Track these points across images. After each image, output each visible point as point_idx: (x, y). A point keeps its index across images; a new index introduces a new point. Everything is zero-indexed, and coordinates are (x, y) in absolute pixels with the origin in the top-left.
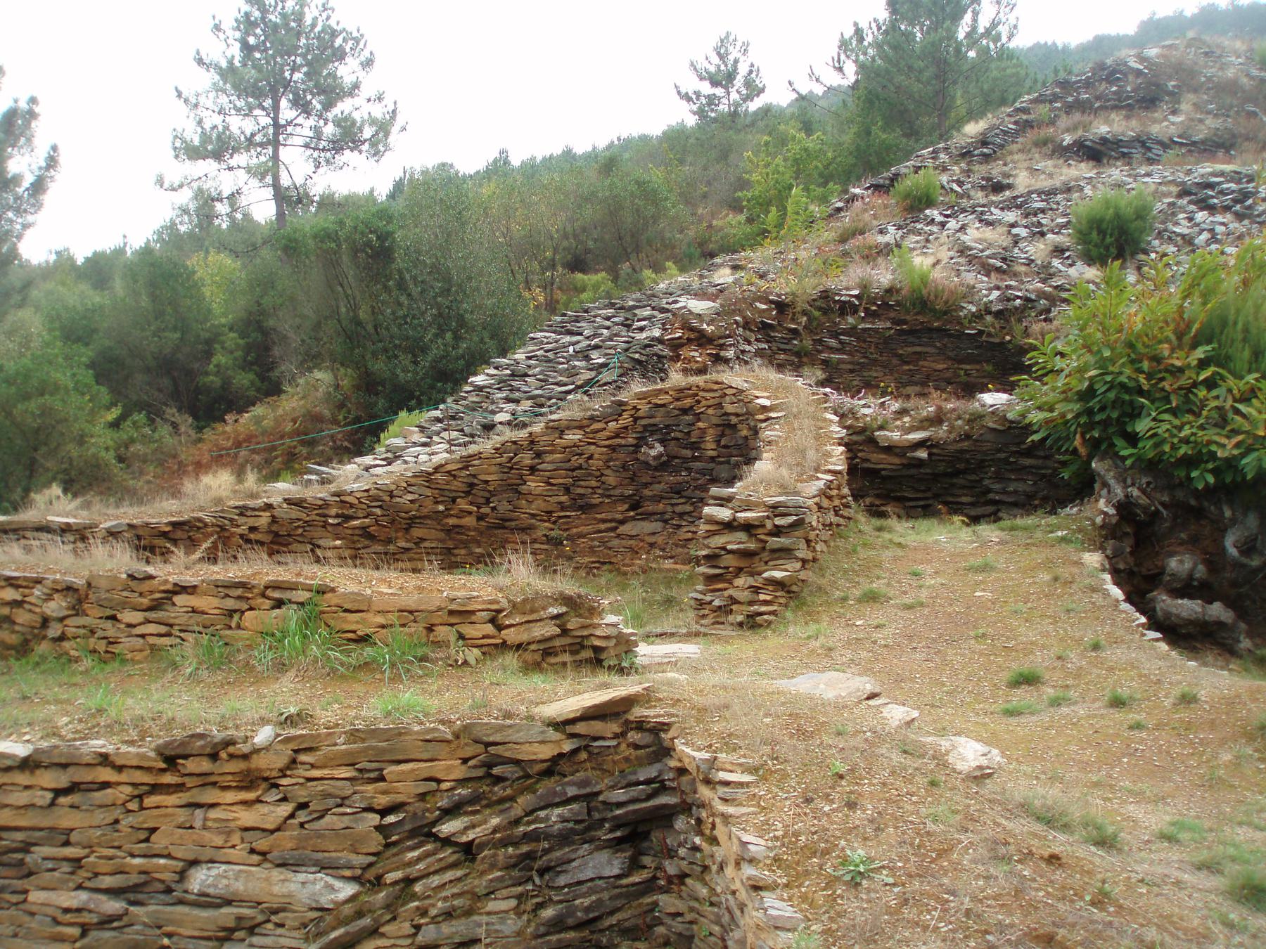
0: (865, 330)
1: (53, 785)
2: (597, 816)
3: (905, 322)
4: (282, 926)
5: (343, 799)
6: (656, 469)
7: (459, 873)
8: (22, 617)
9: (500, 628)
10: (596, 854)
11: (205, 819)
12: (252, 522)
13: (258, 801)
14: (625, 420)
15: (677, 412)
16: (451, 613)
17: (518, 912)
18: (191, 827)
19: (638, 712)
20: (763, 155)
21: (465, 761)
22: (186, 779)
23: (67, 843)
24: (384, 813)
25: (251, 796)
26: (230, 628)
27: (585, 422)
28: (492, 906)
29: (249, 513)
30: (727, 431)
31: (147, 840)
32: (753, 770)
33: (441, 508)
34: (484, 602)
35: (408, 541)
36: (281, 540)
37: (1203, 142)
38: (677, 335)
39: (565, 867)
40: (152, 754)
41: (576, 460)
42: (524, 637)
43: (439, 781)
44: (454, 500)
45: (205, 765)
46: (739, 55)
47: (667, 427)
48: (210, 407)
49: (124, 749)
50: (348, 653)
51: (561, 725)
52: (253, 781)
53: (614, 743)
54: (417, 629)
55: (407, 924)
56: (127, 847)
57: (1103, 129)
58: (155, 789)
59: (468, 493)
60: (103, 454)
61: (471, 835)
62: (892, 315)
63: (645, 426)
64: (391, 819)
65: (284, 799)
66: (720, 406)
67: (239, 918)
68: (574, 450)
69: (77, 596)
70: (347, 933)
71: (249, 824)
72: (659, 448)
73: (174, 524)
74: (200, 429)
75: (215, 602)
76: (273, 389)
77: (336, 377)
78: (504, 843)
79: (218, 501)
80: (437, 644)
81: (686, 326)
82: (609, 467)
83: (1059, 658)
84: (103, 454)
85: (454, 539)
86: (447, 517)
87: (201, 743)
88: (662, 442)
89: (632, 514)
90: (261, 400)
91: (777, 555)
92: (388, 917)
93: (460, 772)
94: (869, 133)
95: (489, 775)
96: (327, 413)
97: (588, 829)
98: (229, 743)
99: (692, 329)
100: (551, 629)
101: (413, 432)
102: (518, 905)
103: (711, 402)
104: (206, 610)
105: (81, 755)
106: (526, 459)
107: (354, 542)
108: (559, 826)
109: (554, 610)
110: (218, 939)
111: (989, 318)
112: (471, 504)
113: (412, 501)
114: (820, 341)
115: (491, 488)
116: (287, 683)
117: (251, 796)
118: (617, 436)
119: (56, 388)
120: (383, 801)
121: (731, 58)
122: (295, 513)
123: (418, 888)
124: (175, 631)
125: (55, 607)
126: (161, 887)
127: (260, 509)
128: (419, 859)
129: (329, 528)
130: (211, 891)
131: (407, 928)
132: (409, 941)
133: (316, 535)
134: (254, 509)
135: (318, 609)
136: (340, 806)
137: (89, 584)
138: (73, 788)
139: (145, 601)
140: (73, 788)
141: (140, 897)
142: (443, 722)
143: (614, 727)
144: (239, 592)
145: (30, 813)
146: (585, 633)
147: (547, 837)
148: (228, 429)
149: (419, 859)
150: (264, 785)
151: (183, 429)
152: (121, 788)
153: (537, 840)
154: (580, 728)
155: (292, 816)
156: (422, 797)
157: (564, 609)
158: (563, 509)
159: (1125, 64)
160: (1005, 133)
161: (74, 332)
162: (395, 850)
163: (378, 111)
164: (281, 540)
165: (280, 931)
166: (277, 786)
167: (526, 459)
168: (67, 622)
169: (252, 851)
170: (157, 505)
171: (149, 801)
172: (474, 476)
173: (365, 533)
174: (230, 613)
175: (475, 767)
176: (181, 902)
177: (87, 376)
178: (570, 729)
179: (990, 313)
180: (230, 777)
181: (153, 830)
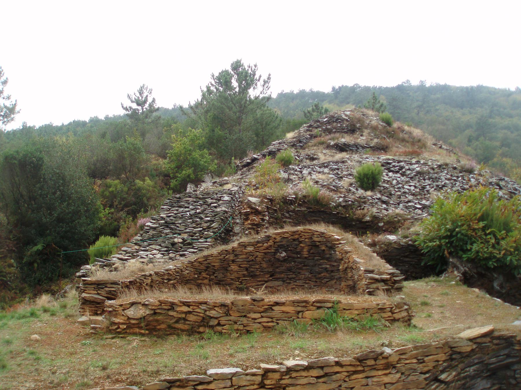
0: (298, 211)
3: (311, 208)
6: (282, 261)
9: (393, 313)
13: (390, 373)
14: (271, 243)
18: (367, 385)
20: (179, 137)
21: (445, 353)
25: (388, 371)
26: (298, 318)
30: (313, 248)
37: (373, 147)
41: (251, 258)
44: (200, 273)
45: (372, 362)
46: (148, 94)
47: (287, 245)
51: (471, 340)
52: (389, 366)
57: (343, 140)
58: (355, 372)
59: (206, 270)
62: (306, 205)
66: (311, 238)
68: (250, 253)
71: (387, 382)
75: (293, 308)
78: (457, 381)
86: (198, 280)
87: (373, 354)
88: (285, 251)
89: (271, 278)
94: (213, 131)
99: (252, 208)
103: (307, 237)
104: (289, 311)
105: (330, 362)
108: (473, 373)
111: (340, 208)
112: (207, 274)
114: (283, 214)
115: (216, 268)
117: (388, 371)
120: (426, 369)
121: (144, 95)
124: (274, 320)
138: (326, 375)
143: (489, 339)
144: (304, 304)
152: (343, 373)
154: (479, 340)
158: (244, 277)
159: (341, 116)
160: (307, 138)
163: (8, 104)
167: (231, 257)
174: (299, 312)
178: (474, 341)
179: (341, 206)
180: (381, 366)
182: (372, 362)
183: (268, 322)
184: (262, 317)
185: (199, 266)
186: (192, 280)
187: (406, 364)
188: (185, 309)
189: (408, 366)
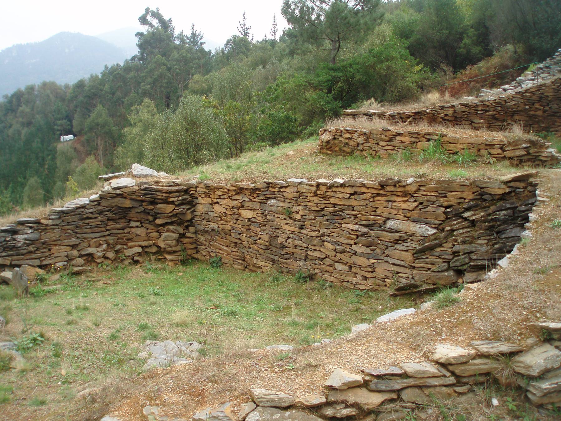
1: (349, 192)
2: (516, 215)
4: (412, 240)
5: (434, 202)
7: (469, 230)
8: (351, 143)
10: (515, 228)
11: (392, 205)
12: (446, 112)
13: (407, 201)
16: (486, 145)
17: (487, 244)
19: (532, 180)
21: (474, 193)
22: (387, 193)
23: (353, 210)
24: (446, 208)
25: (405, 199)
28: (479, 242)
29: (445, 109)
31: (375, 211)
32: (548, 197)
33: (527, 107)
34: (498, 141)
39: (505, 232)
40: (377, 184)
42: (512, 155)
43: (465, 199)
44: (533, 104)
45: (392, 189)
48: (459, 62)
49: (369, 182)
50: (449, 157)
51: (506, 183)
53: (522, 190)
54: (474, 150)
55: (451, 244)
56: (370, 212)
58: (378, 195)
59: (539, 101)
60: (411, 85)
61: (474, 218)
64: (448, 210)
65: (415, 201)
67: (400, 237)
69: (367, 136)
70: (431, 244)
71: (404, 208)
74: (454, 73)
75: (408, 139)
76: (489, 54)
77: (515, 47)
78: (485, 221)
79: (433, 104)
80: (481, 156)
84: (411, 85)
90: (483, 59)
92: (445, 241)
93: (472, 196)
95: (481, 198)
96: (510, 64)
97: (513, 220)
98: (399, 182)
100: (523, 152)
101: (529, 74)
102: (488, 243)
107: (488, 121)
109: (525, 146)
110: (394, 243)
112: (541, 105)
113: (514, 104)
115: (549, 99)
116: (427, 166)
117: (405, 199)
119: (393, 58)
120: (446, 204)
122: (464, 109)
123: (455, 233)
125: (361, 140)
126: (378, 225)
128: (457, 224)
129: (478, 115)
130: (392, 227)
131: (450, 245)
132: (450, 250)
133: (472, 118)
134: (447, 107)
135: (442, 143)
136: (433, 204)
137: (371, 132)
138: (354, 194)
139: (387, 138)
140: (354, 194)
141: (373, 228)
142: (467, 180)
143: (523, 185)
145: (343, 200)
146: (537, 154)
147: (500, 221)
148: (467, 72)
149: (457, 224)
150: (409, 196)
151: (448, 73)
152: (368, 194)
153: (496, 221)
154: (512, 184)
155: (417, 206)
156: (459, 204)
157: (529, 145)
161: (403, 33)
162: (449, 220)
165: (412, 242)
166: (413, 196)
168: (364, 145)
169: (405, 216)
170: (409, 106)
171: (376, 199)
172: (542, 94)
173: (494, 117)
175: (476, 195)
176: (384, 231)
177: (406, 53)
181: (377, 208)
182: (392, 189)
183: (391, 150)
184: (388, 145)
185: (531, 97)
186: (520, 111)
187: (423, 195)
188: (348, 136)
189: (426, 198)
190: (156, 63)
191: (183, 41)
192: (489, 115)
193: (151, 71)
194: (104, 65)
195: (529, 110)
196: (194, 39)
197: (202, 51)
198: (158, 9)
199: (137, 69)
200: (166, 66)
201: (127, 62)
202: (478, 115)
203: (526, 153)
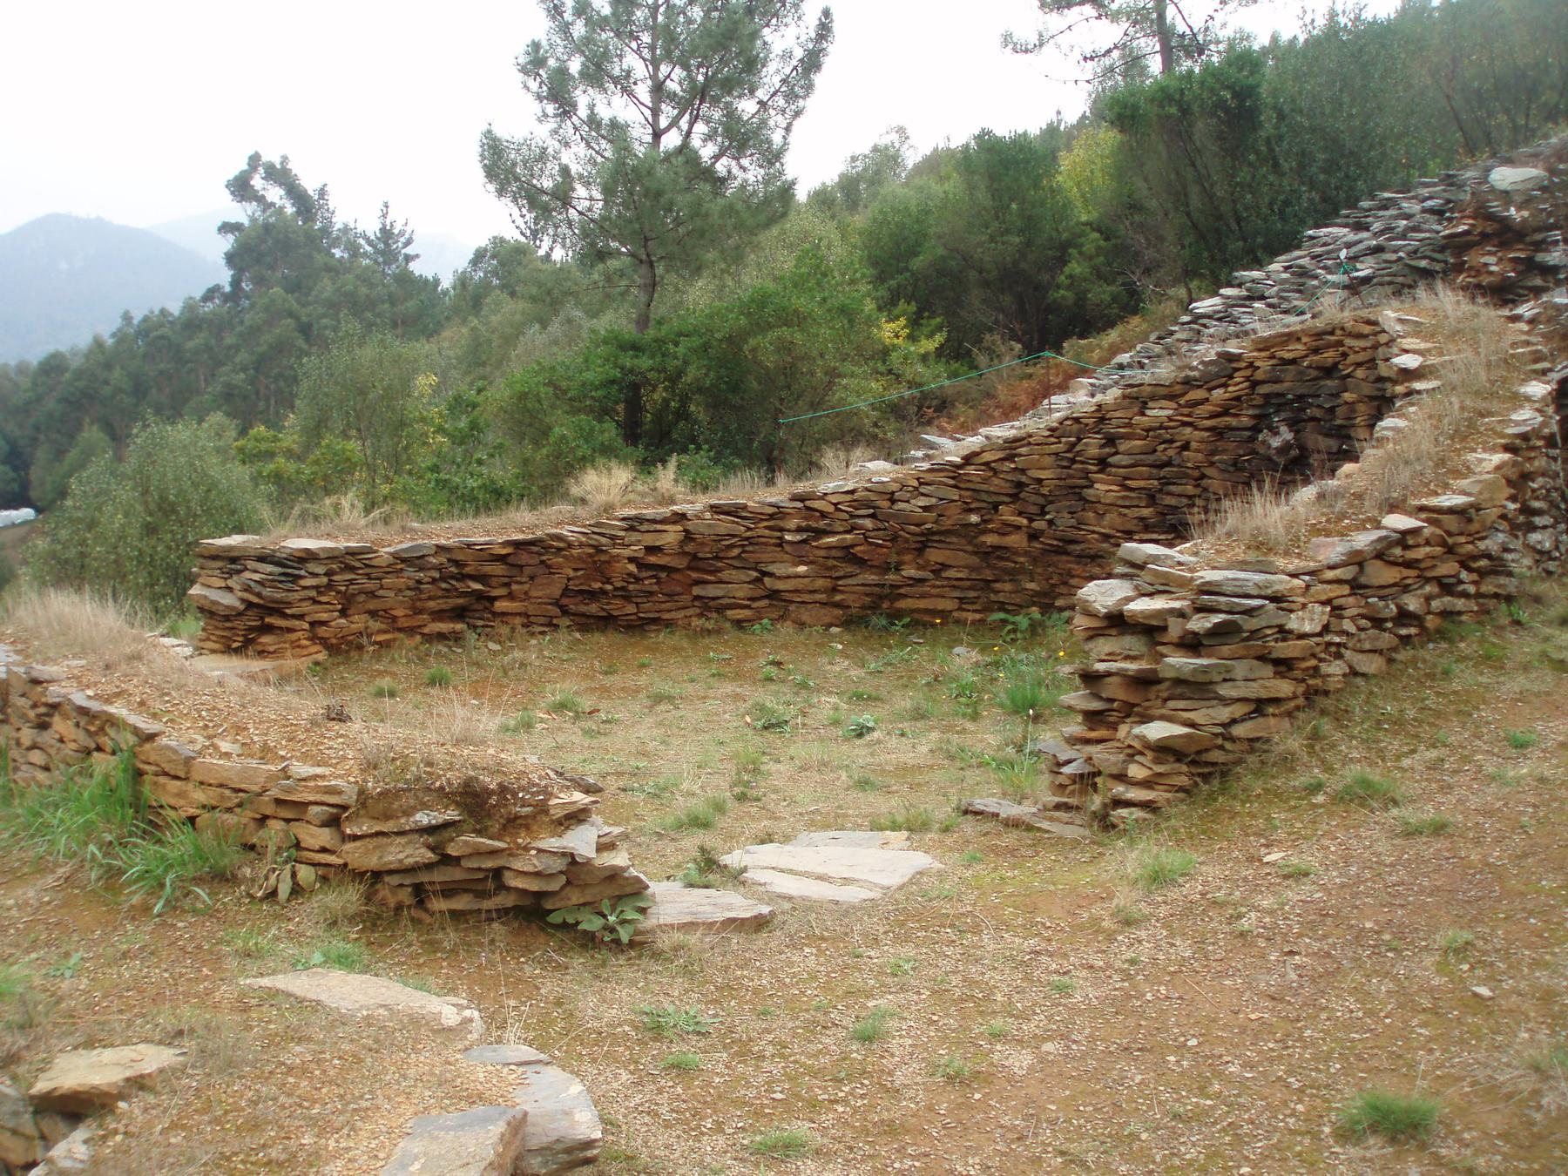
12: (650, 540)
14: (1237, 387)
15: (1314, 373)
27: (1178, 389)
29: (644, 527)
33: (974, 518)
34: (318, 789)
35: (920, 568)
36: (701, 564)
38: (1461, 229)
42: (373, 862)
47: (1300, 398)
59: (1015, 497)
63: (1267, 396)
72: (1286, 434)
73: (517, 545)
81: (1482, 213)
82: (1212, 464)
83: (1537, 1069)
85: (993, 567)
88: (1293, 424)
91: (1179, 691)
99: (1490, 217)
103: (1361, 357)
106: (1092, 446)
109: (423, 818)
112: (1020, 514)
113: (925, 509)
115: (1045, 491)
118: (1225, 413)
127: (663, 521)
129: (788, 548)
133: (764, 557)
134: (654, 521)
164: (701, 564)
167: (1092, 446)
172: (1023, 471)
185: (985, 481)
190: (266, 309)
191: (354, 249)
192: (829, 548)
193: (255, 331)
194: (121, 312)
195: (981, 529)
196: (387, 244)
197: (406, 280)
198: (285, 159)
199: (217, 326)
200: (297, 319)
201: (190, 306)
202: (788, 548)
203: (430, 856)
